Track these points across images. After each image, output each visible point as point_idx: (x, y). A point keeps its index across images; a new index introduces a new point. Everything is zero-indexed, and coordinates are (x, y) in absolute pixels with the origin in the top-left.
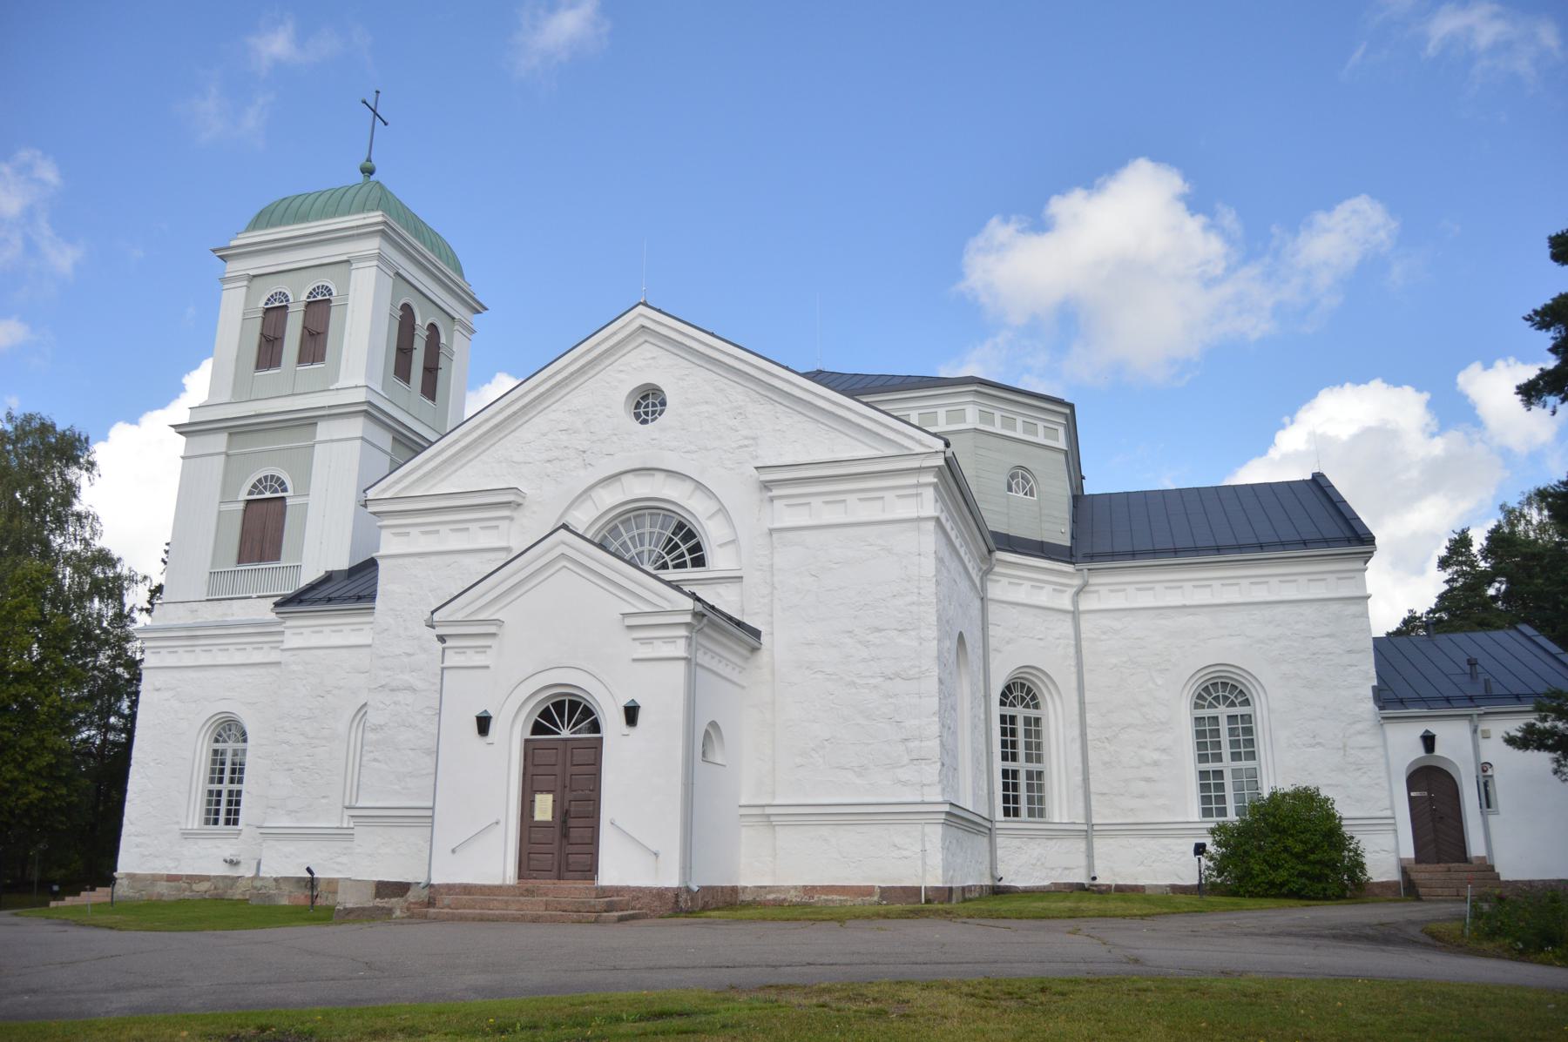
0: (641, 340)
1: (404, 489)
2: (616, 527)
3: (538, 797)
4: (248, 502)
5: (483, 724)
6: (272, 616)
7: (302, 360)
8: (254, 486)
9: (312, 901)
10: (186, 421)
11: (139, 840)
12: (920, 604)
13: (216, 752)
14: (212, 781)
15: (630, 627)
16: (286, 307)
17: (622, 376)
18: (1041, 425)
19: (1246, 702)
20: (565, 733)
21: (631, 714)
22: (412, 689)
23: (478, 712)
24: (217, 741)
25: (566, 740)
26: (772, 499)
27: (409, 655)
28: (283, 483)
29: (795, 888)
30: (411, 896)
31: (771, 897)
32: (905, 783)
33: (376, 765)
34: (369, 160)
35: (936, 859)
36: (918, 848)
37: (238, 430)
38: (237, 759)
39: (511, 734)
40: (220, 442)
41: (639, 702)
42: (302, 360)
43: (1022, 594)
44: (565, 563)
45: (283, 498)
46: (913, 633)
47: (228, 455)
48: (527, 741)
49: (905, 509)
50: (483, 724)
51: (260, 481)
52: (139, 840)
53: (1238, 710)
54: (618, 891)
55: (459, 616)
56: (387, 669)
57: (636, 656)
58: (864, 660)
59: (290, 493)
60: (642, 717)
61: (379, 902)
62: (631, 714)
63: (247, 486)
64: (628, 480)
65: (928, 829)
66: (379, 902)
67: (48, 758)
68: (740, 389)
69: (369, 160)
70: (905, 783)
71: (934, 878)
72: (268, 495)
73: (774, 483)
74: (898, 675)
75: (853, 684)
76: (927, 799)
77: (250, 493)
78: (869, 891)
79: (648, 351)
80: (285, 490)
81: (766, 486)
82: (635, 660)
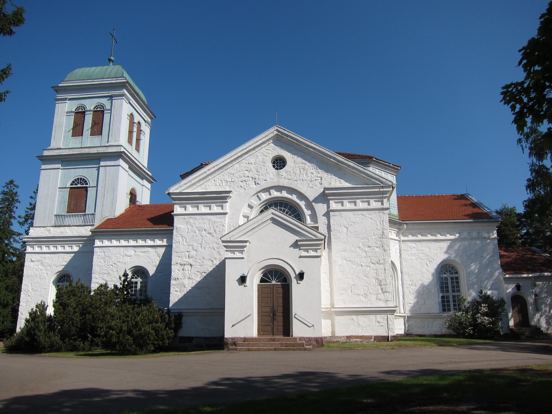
3: (52, 314)
4: (71, 188)
5: (243, 280)
8: (73, 182)
9: (319, 342)
17: (269, 152)
19: (457, 273)
20: (274, 282)
25: (273, 285)
29: (344, 337)
39: (254, 281)
41: (304, 271)
45: (87, 188)
53: (454, 276)
63: (70, 182)
67: (471, 282)
72: (79, 185)
76: (389, 306)
77: (72, 184)
78: (369, 337)
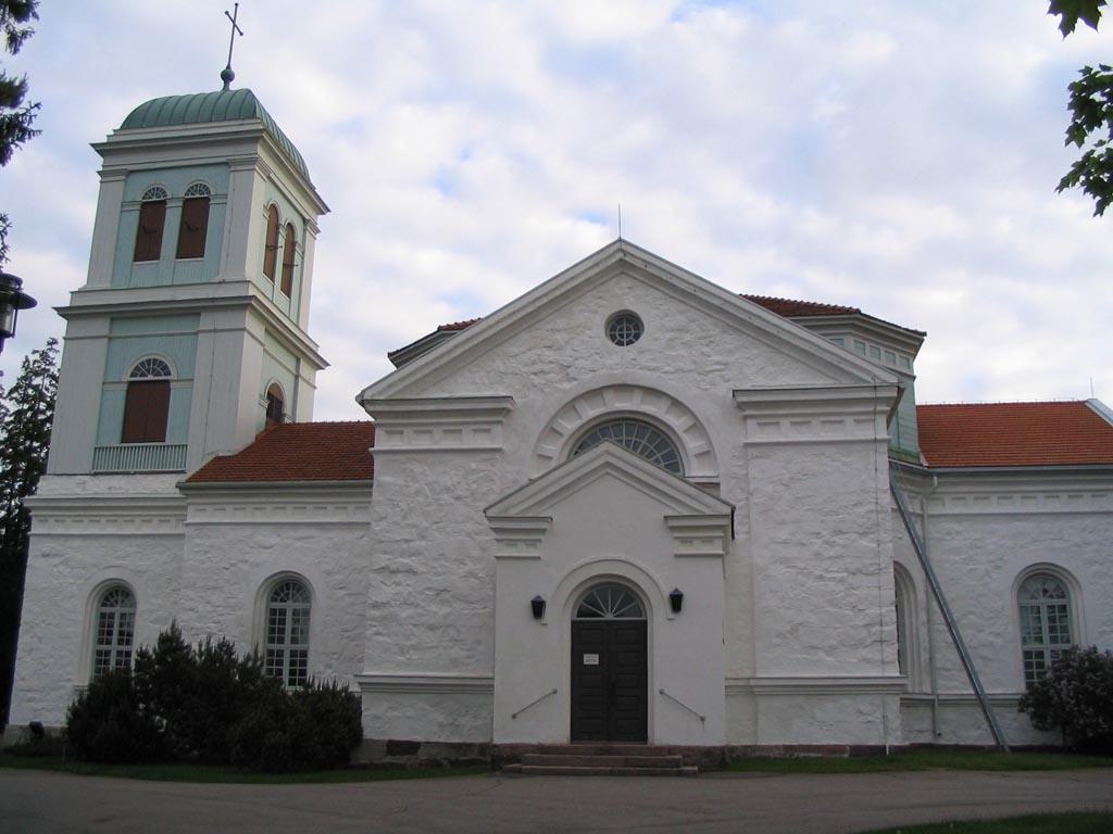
0: (618, 272)
1: (400, 391)
2: (596, 433)
5: (538, 608)
6: (177, 493)
7: (179, 256)
10: (68, 305)
11: (30, 695)
12: (877, 512)
13: (103, 615)
14: (100, 642)
15: (673, 529)
16: (164, 202)
18: (897, 356)
20: (609, 617)
21: (676, 601)
22: (411, 572)
23: (532, 597)
24: (104, 605)
26: (745, 418)
27: (407, 541)
28: (166, 367)
29: (777, 747)
30: (422, 755)
31: (758, 754)
32: (867, 661)
33: (381, 638)
34: (229, 67)
35: (895, 721)
36: (879, 714)
37: (118, 315)
38: (125, 629)
39: (560, 621)
40: (101, 327)
41: (682, 591)
42: (179, 256)
43: (396, 443)
44: (609, 470)
45: (167, 382)
46: (872, 536)
47: (110, 339)
48: (574, 623)
49: (865, 433)
50: (538, 608)
51: (155, 360)
52: (30, 695)
54: (671, 750)
55: (512, 513)
56: (385, 553)
57: (678, 553)
58: (830, 558)
59: (173, 376)
60: (685, 604)
61: (389, 759)
62: (676, 601)
64: (609, 396)
65: (889, 698)
66: (389, 759)
68: (711, 320)
69: (229, 67)
70: (867, 661)
71: (893, 741)
73: (752, 405)
74: (860, 571)
75: (821, 577)
77: (133, 375)
79: (626, 283)
80: (169, 374)
81: (741, 406)
82: (676, 556)
